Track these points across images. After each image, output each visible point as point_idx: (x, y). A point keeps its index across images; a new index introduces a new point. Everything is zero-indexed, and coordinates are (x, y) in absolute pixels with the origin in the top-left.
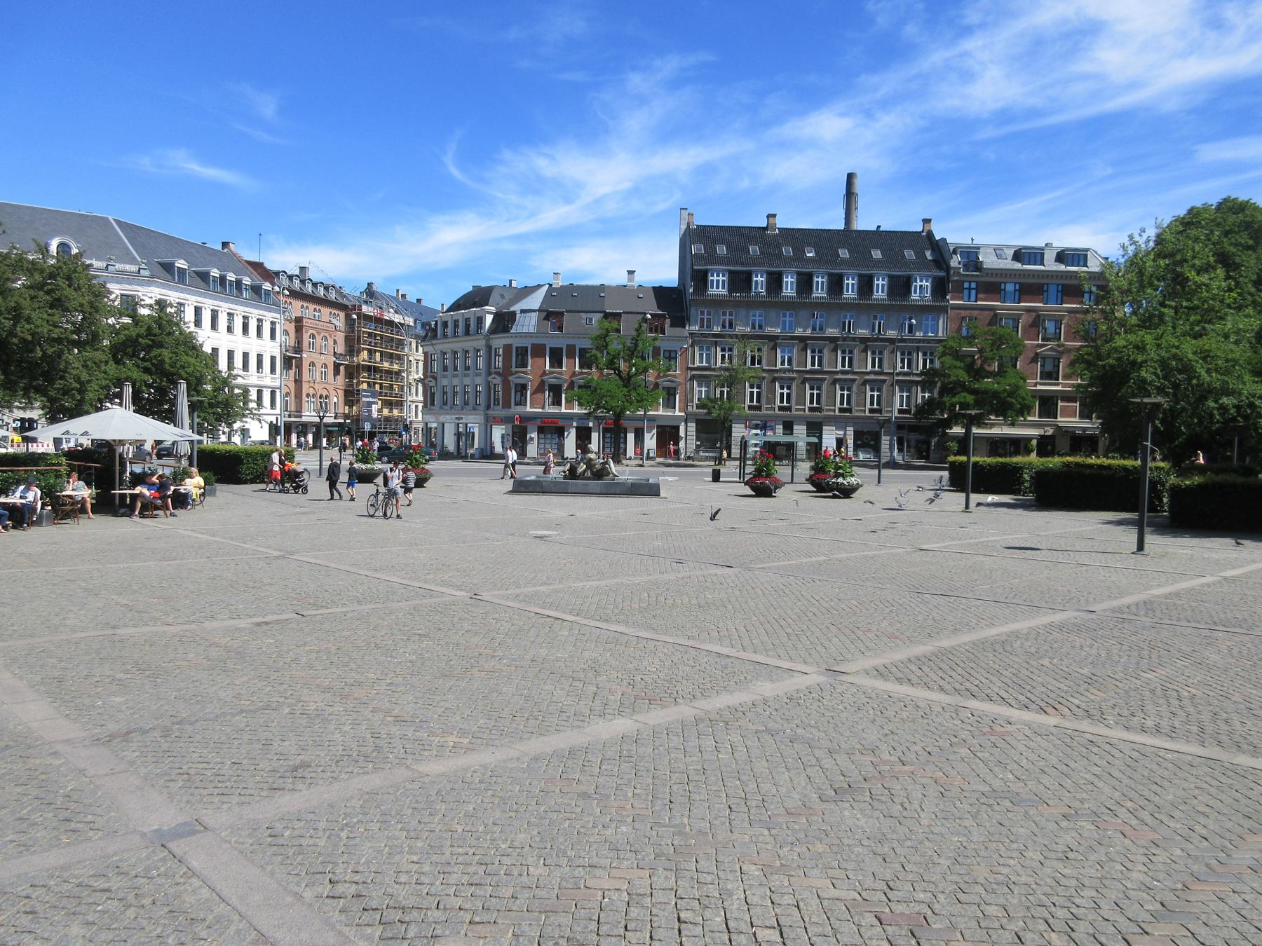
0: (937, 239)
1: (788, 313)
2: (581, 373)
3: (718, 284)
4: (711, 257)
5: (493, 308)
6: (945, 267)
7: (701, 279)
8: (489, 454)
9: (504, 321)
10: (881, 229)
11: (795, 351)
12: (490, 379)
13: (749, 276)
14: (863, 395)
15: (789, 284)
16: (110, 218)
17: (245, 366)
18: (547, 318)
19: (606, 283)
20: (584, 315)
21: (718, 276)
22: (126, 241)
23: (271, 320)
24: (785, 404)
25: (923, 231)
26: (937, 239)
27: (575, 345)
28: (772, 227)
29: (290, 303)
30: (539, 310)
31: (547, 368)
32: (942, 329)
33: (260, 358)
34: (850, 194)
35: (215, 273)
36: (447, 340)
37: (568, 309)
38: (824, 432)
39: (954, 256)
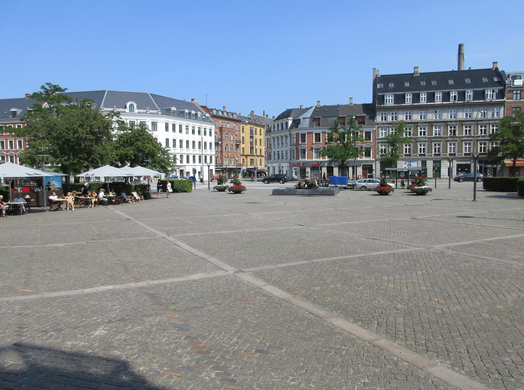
0: (500, 71)
1: (468, 110)
2: (315, 144)
3: (390, 100)
4: (387, 90)
6: (503, 84)
7: (382, 99)
8: (291, 179)
9: (296, 123)
10: (471, 69)
11: (427, 128)
13: (404, 96)
15: (469, 93)
16: (149, 93)
17: (174, 146)
18: (314, 120)
19: (327, 105)
20: (329, 119)
21: (389, 97)
22: (154, 101)
23: (210, 128)
25: (493, 68)
26: (500, 71)
28: (416, 73)
29: (224, 122)
30: (310, 118)
31: (314, 142)
33: (194, 142)
34: (460, 54)
35: (187, 111)
38: (442, 163)
39: (508, 78)
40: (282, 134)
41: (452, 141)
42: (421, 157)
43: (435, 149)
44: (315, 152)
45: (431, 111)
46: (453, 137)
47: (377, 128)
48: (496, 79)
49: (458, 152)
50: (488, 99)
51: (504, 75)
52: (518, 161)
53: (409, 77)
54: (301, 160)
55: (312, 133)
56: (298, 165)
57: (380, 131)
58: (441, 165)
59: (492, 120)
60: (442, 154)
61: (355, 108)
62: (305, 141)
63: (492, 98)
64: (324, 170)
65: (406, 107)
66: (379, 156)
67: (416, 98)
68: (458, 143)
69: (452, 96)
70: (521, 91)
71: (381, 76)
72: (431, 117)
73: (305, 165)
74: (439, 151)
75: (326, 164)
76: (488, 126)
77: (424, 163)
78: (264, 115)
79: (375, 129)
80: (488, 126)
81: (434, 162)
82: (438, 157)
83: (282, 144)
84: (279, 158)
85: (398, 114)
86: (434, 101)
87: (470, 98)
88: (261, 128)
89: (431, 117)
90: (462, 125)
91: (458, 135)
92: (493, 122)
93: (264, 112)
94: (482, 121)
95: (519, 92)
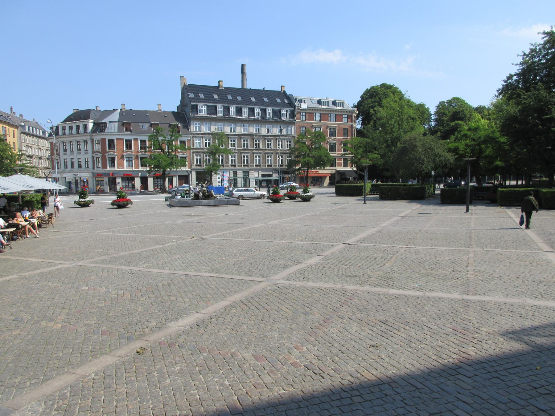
5: (93, 120)
6: (293, 106)
7: (195, 109)
9: (100, 127)
10: (265, 89)
11: (236, 141)
12: (94, 155)
13: (215, 108)
14: (265, 159)
20: (141, 124)
21: (202, 107)
24: (198, 164)
27: (105, 138)
32: (291, 131)
34: (243, 73)
36: (79, 135)
37: (133, 121)
38: (250, 174)
40: (78, 139)
41: (257, 153)
42: (232, 168)
43: (244, 160)
44: (126, 161)
45: (239, 124)
46: (258, 150)
47: (192, 138)
48: (286, 101)
49: (263, 163)
50: (284, 118)
51: (292, 98)
52: (310, 172)
53: (216, 89)
54: (109, 169)
55: (122, 139)
56: (107, 174)
57: (195, 141)
58: (250, 175)
59: (287, 136)
60: (249, 165)
61: (166, 116)
62: (131, 148)
63: (287, 117)
64: (138, 182)
65: (218, 119)
66: (195, 166)
67: (227, 110)
68: (262, 155)
69: (256, 112)
70: (305, 113)
71: (188, 84)
72: (240, 130)
73: (115, 175)
74: (247, 163)
75: (140, 174)
76: (284, 141)
77: (235, 173)
78: (11, 112)
79: (189, 139)
80: (284, 141)
81: (244, 172)
82: (247, 168)
83: (79, 150)
84: (73, 167)
85: (211, 126)
86: (216, 115)
87: (270, 115)
88: (14, 129)
89: (240, 130)
90: (265, 139)
91: (262, 148)
92: (287, 138)
93: (11, 109)
94: (279, 136)
95: (304, 114)
